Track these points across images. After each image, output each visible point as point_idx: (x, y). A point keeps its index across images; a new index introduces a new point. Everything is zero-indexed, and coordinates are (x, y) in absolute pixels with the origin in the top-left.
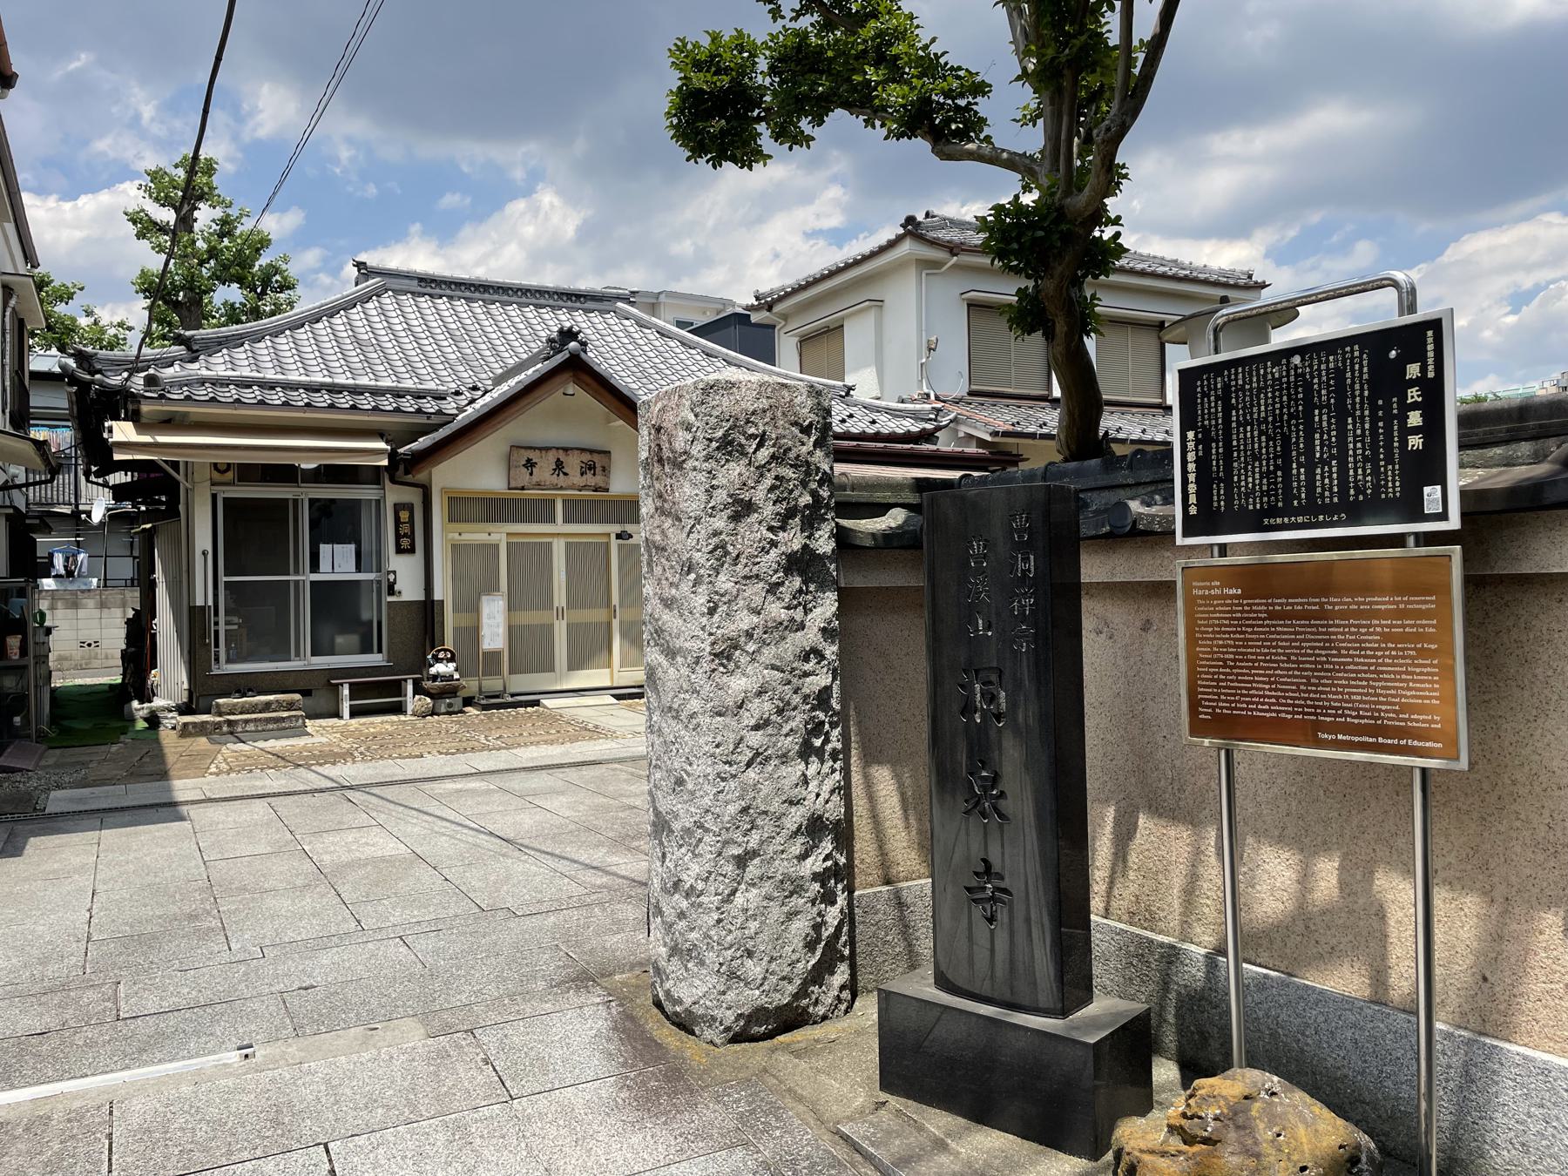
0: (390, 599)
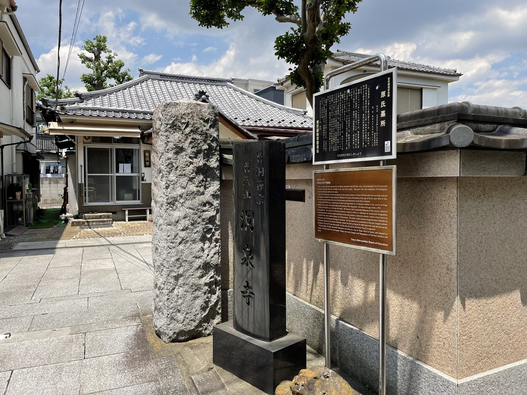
0: (143, 182)
